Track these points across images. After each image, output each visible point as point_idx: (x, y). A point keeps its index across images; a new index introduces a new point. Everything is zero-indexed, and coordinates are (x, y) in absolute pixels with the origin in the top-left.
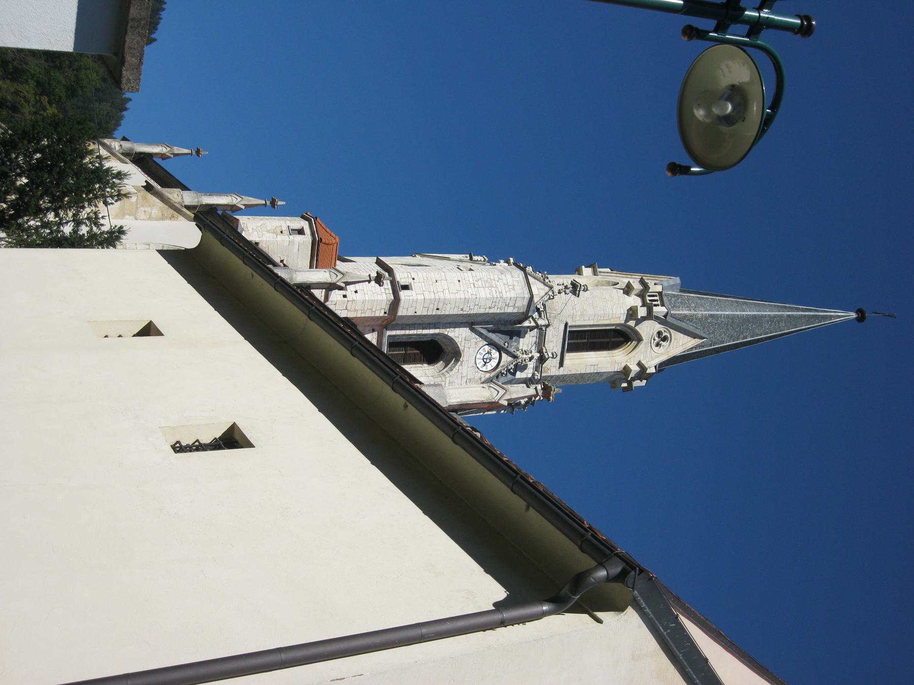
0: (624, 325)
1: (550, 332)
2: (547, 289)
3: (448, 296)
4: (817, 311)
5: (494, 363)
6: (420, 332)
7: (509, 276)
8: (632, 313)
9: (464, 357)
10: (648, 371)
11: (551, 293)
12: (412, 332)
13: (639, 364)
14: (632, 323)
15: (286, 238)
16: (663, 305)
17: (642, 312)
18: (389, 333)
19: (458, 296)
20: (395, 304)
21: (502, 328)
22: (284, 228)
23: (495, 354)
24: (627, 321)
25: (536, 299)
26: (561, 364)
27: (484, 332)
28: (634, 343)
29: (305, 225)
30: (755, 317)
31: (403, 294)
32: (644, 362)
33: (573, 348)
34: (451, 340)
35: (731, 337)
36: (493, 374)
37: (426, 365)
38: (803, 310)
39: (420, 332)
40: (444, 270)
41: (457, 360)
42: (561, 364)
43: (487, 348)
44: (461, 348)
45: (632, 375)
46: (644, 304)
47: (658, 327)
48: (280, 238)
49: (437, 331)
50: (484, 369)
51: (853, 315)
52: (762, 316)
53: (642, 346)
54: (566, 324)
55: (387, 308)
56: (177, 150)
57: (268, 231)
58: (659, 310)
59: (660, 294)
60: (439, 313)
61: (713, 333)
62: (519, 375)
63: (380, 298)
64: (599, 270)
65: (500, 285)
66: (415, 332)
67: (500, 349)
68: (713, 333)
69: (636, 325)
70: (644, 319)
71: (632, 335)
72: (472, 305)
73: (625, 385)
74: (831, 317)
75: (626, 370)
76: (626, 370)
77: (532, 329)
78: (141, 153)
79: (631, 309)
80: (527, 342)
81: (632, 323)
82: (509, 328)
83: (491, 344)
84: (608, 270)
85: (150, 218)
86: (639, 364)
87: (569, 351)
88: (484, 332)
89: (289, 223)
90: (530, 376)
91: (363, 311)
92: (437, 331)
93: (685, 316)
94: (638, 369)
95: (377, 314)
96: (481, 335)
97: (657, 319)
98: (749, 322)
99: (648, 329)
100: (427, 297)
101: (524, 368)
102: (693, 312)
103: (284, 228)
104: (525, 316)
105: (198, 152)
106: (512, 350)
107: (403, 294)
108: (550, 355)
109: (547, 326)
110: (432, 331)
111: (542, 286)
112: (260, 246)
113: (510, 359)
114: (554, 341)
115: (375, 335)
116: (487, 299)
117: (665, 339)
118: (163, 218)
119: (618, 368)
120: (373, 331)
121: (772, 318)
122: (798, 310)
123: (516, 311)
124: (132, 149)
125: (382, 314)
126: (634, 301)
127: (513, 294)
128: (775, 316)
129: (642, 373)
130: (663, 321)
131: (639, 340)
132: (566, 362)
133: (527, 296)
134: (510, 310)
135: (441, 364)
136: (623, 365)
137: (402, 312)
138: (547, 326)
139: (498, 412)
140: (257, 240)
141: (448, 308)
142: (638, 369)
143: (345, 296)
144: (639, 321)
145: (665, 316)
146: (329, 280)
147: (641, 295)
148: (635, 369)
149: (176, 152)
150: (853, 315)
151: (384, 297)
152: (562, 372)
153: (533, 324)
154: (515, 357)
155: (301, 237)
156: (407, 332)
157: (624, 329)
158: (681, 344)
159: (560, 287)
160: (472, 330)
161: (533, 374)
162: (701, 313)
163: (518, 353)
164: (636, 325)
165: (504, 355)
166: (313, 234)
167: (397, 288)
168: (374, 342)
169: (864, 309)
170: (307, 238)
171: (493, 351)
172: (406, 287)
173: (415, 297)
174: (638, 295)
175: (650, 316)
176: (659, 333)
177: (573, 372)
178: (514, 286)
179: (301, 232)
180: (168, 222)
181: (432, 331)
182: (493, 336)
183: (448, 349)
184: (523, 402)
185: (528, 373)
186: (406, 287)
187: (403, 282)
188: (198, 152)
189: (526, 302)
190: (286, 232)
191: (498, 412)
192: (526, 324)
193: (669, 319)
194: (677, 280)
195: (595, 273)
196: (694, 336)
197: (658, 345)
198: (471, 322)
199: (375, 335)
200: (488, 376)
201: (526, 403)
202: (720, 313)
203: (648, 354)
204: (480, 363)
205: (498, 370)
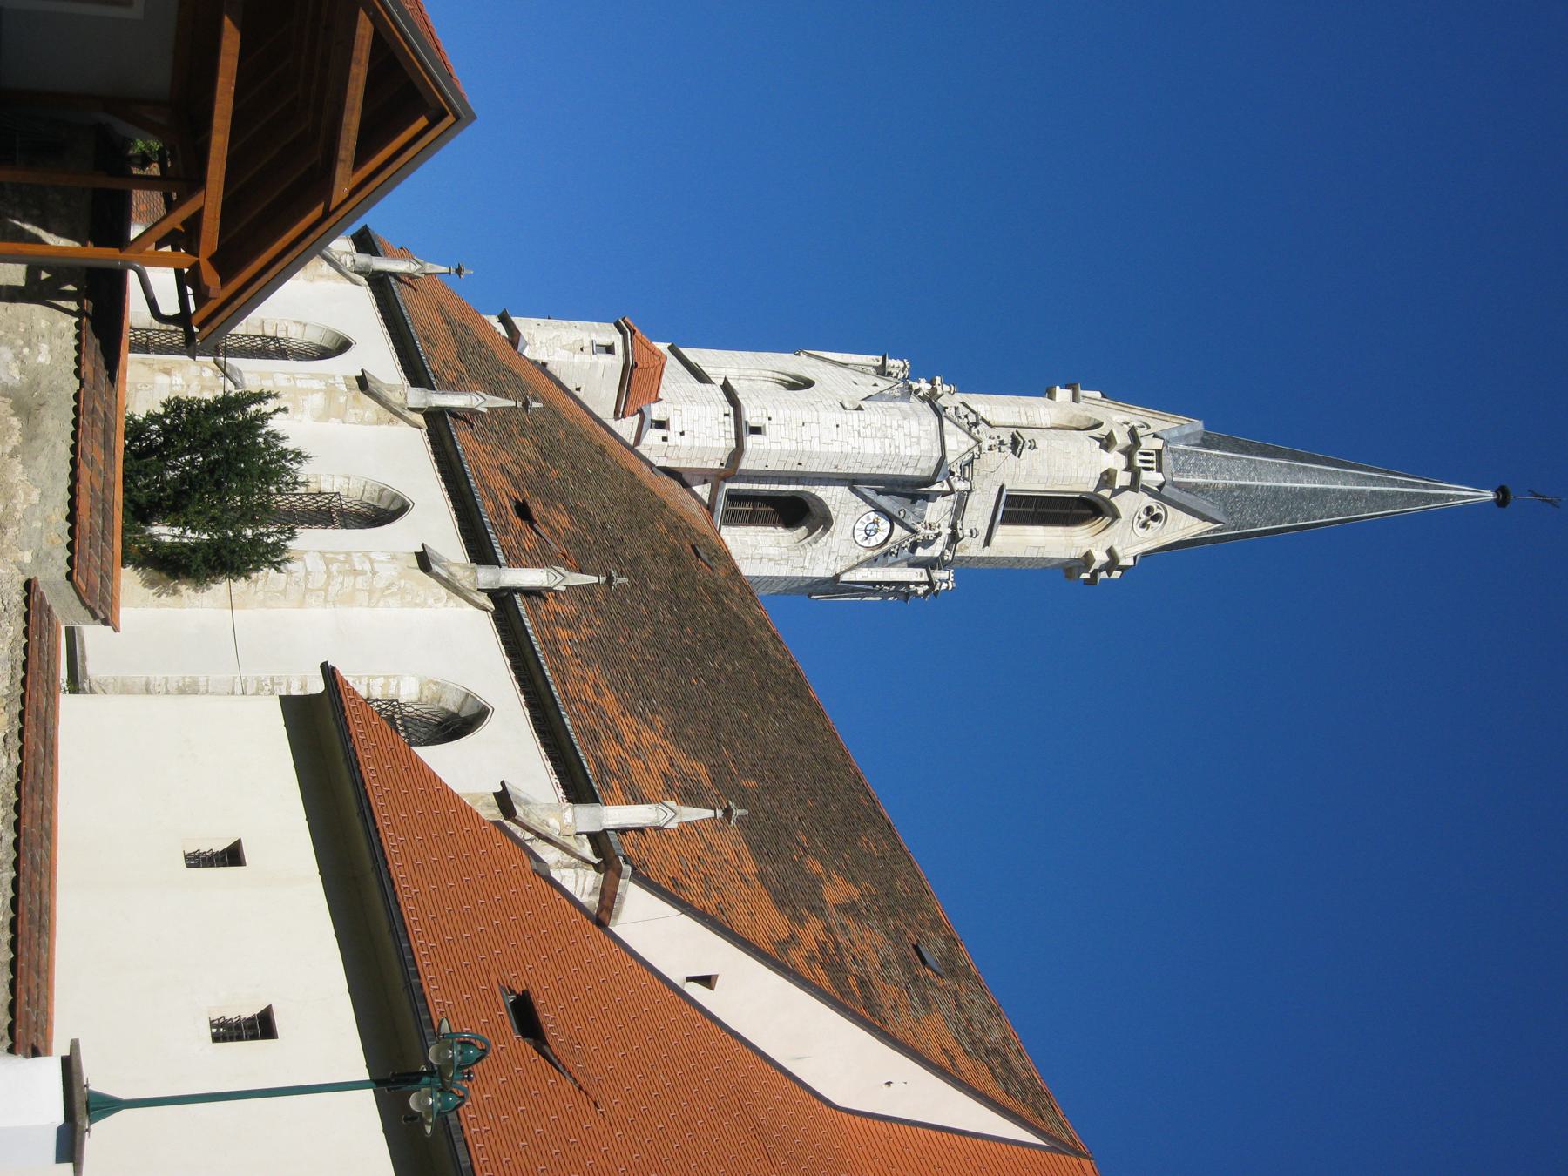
0: (1094, 494)
1: (973, 500)
2: (973, 442)
3: (816, 448)
4: (1426, 486)
5: (881, 537)
6: (774, 487)
7: (914, 423)
8: (1107, 478)
9: (836, 527)
10: (1122, 563)
11: (976, 450)
12: (762, 487)
13: (1110, 552)
14: (1106, 493)
15: (586, 358)
16: (1159, 470)
17: (1123, 479)
18: (728, 486)
19: (831, 449)
20: (738, 453)
21: (899, 490)
22: (586, 344)
23: (885, 525)
24: (1098, 488)
25: (950, 458)
26: (987, 542)
27: (870, 494)
28: (1107, 520)
29: (616, 339)
30: (1314, 491)
31: (751, 441)
32: (1117, 549)
33: (1009, 519)
34: (820, 500)
35: (1269, 520)
36: (878, 552)
37: (780, 529)
38: (1401, 484)
39: (774, 487)
40: (820, 406)
41: (826, 529)
42: (987, 542)
43: (873, 516)
44: (833, 514)
45: (1096, 566)
46: (1130, 467)
47: (1147, 500)
48: (578, 358)
49: (800, 488)
50: (865, 544)
51: (1490, 495)
52: (1328, 490)
53: (1118, 525)
54: (1002, 488)
55: (724, 461)
56: (431, 268)
57: (563, 347)
58: (1151, 478)
59: (1159, 452)
60: (801, 469)
61: (1241, 511)
62: (920, 552)
63: (716, 444)
64: (1082, 393)
65: (899, 438)
66: (767, 487)
67: (892, 519)
68: (1241, 511)
69: (1113, 495)
70: (1123, 489)
71: (1105, 507)
72: (851, 462)
73: (1085, 576)
74: (1448, 497)
75: (1088, 558)
76: (1088, 558)
77: (944, 494)
78: (380, 272)
79: (1107, 472)
80: (937, 512)
81: (1106, 493)
82: (911, 491)
83: (880, 510)
84: (1098, 394)
85: (362, 422)
86: (1110, 552)
87: (1004, 521)
88: (870, 494)
89: (594, 337)
90: (937, 554)
91: (689, 460)
92: (800, 488)
93: (1197, 485)
94: (1106, 558)
95: (710, 466)
96: (865, 498)
97: (1146, 489)
98: (1304, 498)
99: (1130, 504)
100: (785, 447)
101: (927, 543)
102: (1210, 480)
103: (586, 344)
104: (930, 481)
105: (459, 271)
106: (909, 522)
107: (751, 441)
108: (967, 532)
109: (970, 491)
110: (792, 488)
111: (965, 437)
112: (549, 368)
113: (906, 533)
114: (979, 512)
115: (708, 487)
116: (875, 455)
117: (1156, 518)
118: (379, 422)
119: (1076, 553)
120: (706, 482)
121: (1344, 495)
122: (1392, 483)
123: (917, 473)
124: (368, 266)
125: (717, 466)
126: (1115, 461)
127: (915, 451)
128: (1350, 492)
129: (1113, 563)
130: (1157, 493)
131: (1116, 516)
132: (996, 539)
133: (937, 455)
134: (909, 472)
135: (803, 530)
136: (1085, 551)
137: (746, 464)
138: (970, 491)
139: (885, 598)
140: (545, 359)
141: (815, 463)
142: (1106, 558)
143: (665, 439)
144: (1116, 493)
145: (1160, 487)
146: (546, 584)
147: (1129, 453)
148: (1101, 557)
149: (429, 271)
150: (1490, 495)
151: (722, 444)
152: (987, 552)
153: (946, 488)
154: (914, 532)
155: (609, 357)
156: (756, 486)
157: (1094, 499)
158: (1181, 527)
159: (993, 442)
160: (853, 490)
161: (943, 553)
162: (1224, 481)
163: (919, 527)
164: (1113, 495)
165: (897, 528)
166: (626, 354)
167: (743, 430)
168: (706, 498)
169: (1510, 489)
170: (617, 361)
171: (882, 521)
172: (756, 430)
173: (767, 447)
174: (1123, 452)
175: (1134, 485)
176: (1149, 509)
177: (1005, 555)
178: (919, 438)
179: (610, 350)
180: (384, 427)
181: (792, 488)
182: (884, 501)
183: (815, 510)
184: (921, 590)
185: (934, 551)
186: (756, 430)
187: (754, 423)
188: (459, 271)
189: (934, 464)
190: (588, 350)
191: (885, 598)
192: (936, 487)
193: (1164, 492)
194: (1199, 425)
195: (1075, 399)
196: (1205, 518)
197: (1144, 525)
198: (852, 482)
199: (708, 487)
200: (869, 553)
201: (926, 592)
202: (1256, 483)
203: (1128, 538)
204: (860, 535)
205: (885, 548)
